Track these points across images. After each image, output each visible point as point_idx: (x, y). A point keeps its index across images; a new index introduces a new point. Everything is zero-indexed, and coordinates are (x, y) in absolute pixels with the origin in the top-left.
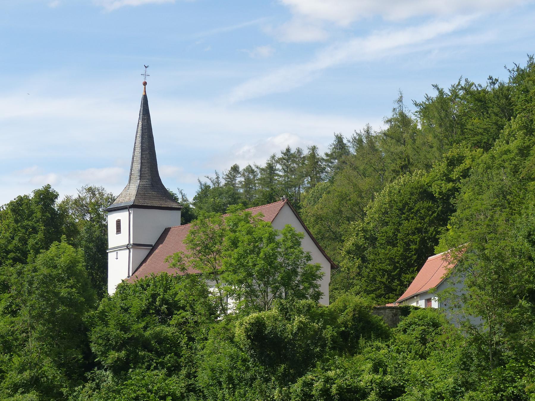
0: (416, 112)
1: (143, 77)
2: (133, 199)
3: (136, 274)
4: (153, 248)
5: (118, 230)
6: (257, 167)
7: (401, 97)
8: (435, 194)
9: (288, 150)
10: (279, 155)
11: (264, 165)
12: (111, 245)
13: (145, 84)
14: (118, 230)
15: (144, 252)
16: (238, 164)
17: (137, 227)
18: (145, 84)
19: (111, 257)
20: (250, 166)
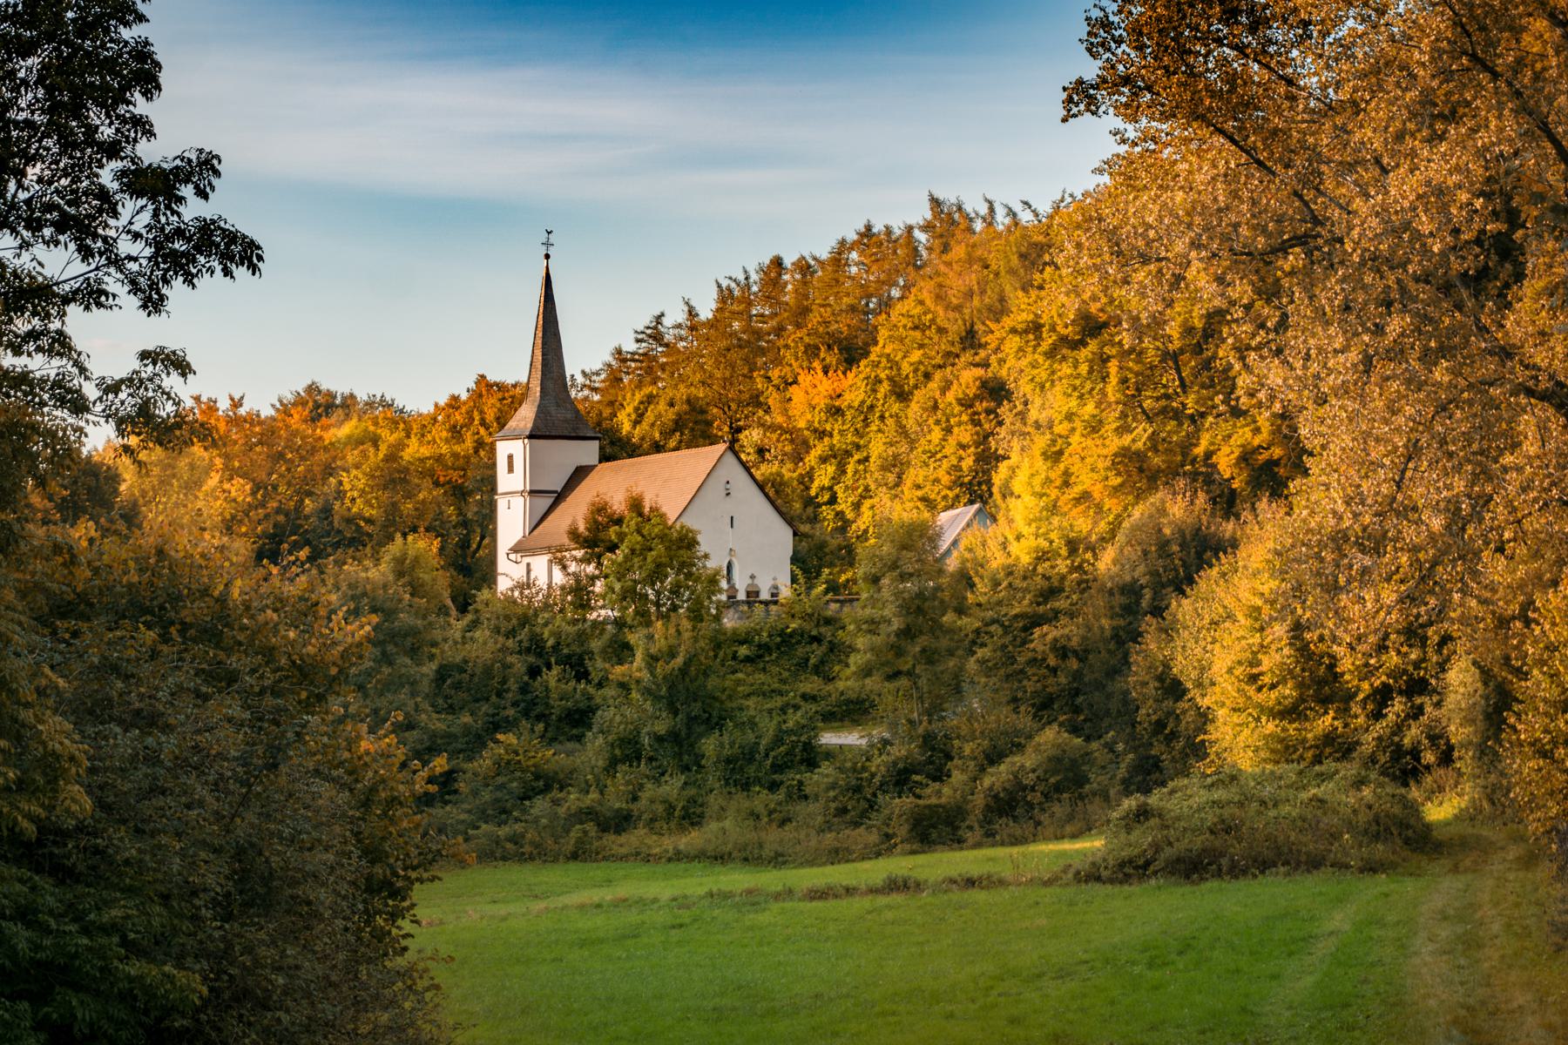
0: (1071, 195)
1: (544, 247)
2: (530, 425)
3: (535, 533)
4: (560, 497)
5: (511, 469)
6: (815, 259)
7: (1010, 209)
8: (363, 1023)
9: (869, 228)
10: (852, 237)
11: (824, 255)
12: (501, 488)
13: (547, 257)
14: (511, 469)
15: (546, 502)
16: (782, 255)
17: (535, 466)
18: (547, 257)
19: (502, 504)
20: (804, 258)
